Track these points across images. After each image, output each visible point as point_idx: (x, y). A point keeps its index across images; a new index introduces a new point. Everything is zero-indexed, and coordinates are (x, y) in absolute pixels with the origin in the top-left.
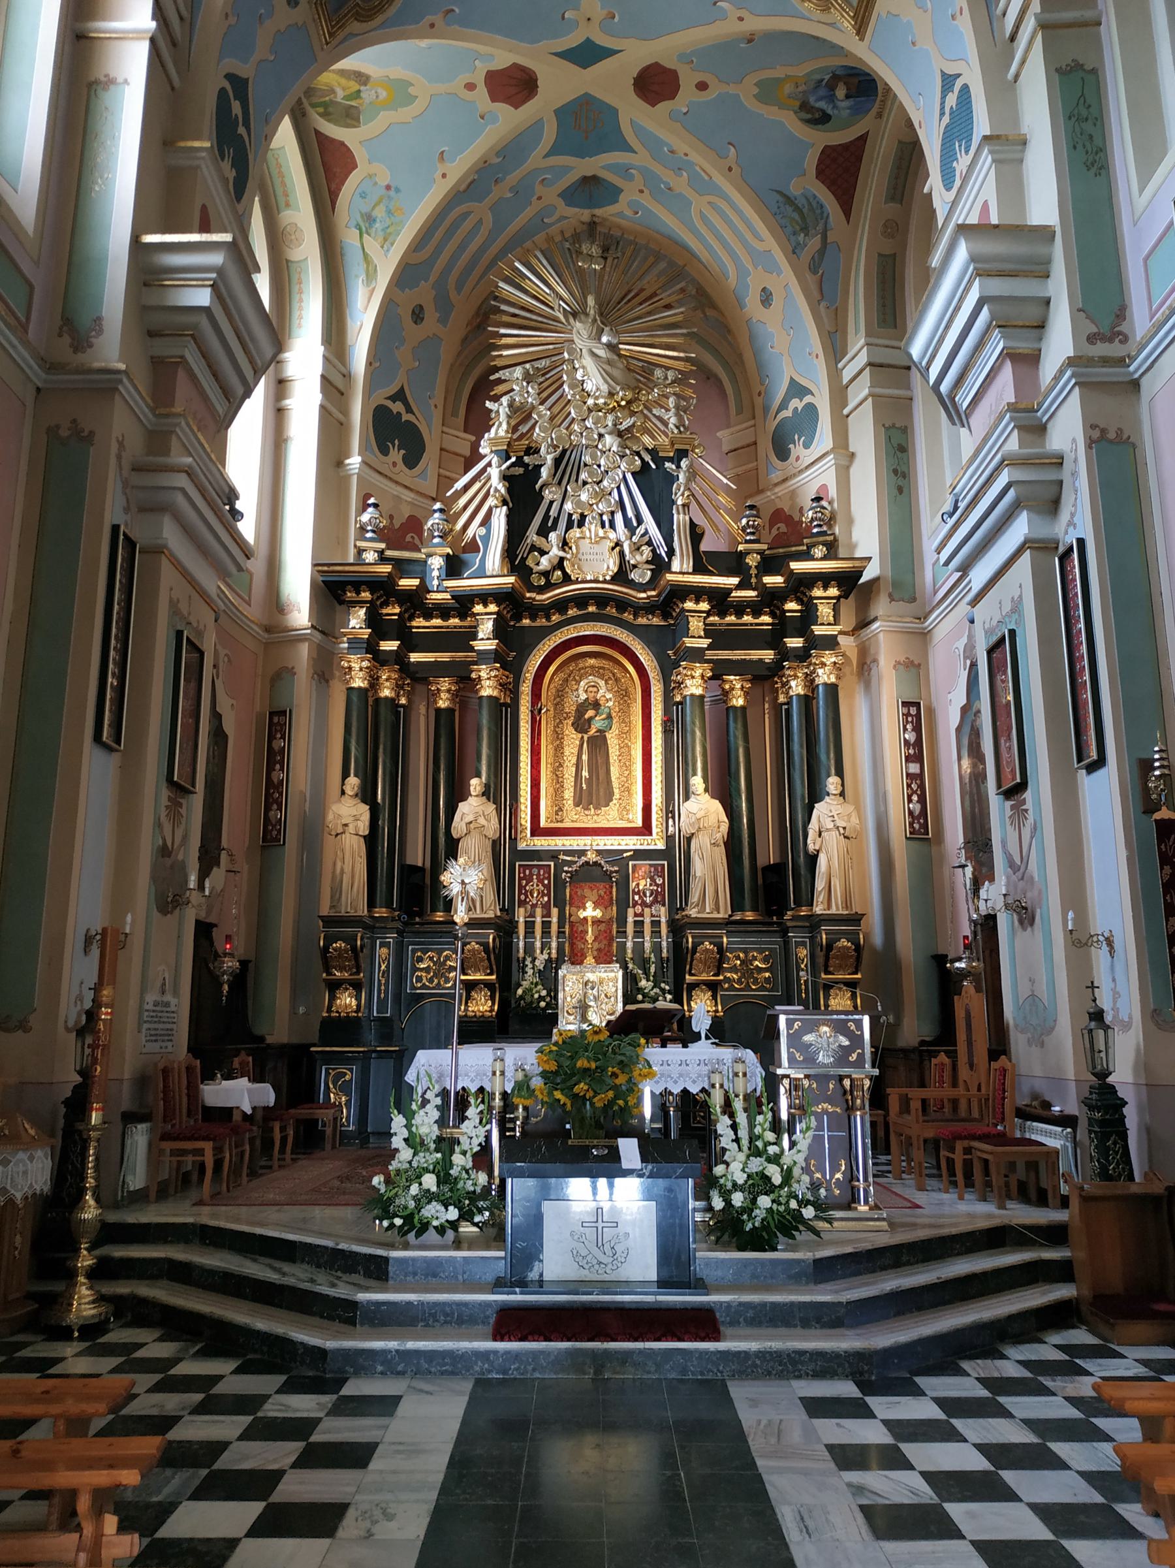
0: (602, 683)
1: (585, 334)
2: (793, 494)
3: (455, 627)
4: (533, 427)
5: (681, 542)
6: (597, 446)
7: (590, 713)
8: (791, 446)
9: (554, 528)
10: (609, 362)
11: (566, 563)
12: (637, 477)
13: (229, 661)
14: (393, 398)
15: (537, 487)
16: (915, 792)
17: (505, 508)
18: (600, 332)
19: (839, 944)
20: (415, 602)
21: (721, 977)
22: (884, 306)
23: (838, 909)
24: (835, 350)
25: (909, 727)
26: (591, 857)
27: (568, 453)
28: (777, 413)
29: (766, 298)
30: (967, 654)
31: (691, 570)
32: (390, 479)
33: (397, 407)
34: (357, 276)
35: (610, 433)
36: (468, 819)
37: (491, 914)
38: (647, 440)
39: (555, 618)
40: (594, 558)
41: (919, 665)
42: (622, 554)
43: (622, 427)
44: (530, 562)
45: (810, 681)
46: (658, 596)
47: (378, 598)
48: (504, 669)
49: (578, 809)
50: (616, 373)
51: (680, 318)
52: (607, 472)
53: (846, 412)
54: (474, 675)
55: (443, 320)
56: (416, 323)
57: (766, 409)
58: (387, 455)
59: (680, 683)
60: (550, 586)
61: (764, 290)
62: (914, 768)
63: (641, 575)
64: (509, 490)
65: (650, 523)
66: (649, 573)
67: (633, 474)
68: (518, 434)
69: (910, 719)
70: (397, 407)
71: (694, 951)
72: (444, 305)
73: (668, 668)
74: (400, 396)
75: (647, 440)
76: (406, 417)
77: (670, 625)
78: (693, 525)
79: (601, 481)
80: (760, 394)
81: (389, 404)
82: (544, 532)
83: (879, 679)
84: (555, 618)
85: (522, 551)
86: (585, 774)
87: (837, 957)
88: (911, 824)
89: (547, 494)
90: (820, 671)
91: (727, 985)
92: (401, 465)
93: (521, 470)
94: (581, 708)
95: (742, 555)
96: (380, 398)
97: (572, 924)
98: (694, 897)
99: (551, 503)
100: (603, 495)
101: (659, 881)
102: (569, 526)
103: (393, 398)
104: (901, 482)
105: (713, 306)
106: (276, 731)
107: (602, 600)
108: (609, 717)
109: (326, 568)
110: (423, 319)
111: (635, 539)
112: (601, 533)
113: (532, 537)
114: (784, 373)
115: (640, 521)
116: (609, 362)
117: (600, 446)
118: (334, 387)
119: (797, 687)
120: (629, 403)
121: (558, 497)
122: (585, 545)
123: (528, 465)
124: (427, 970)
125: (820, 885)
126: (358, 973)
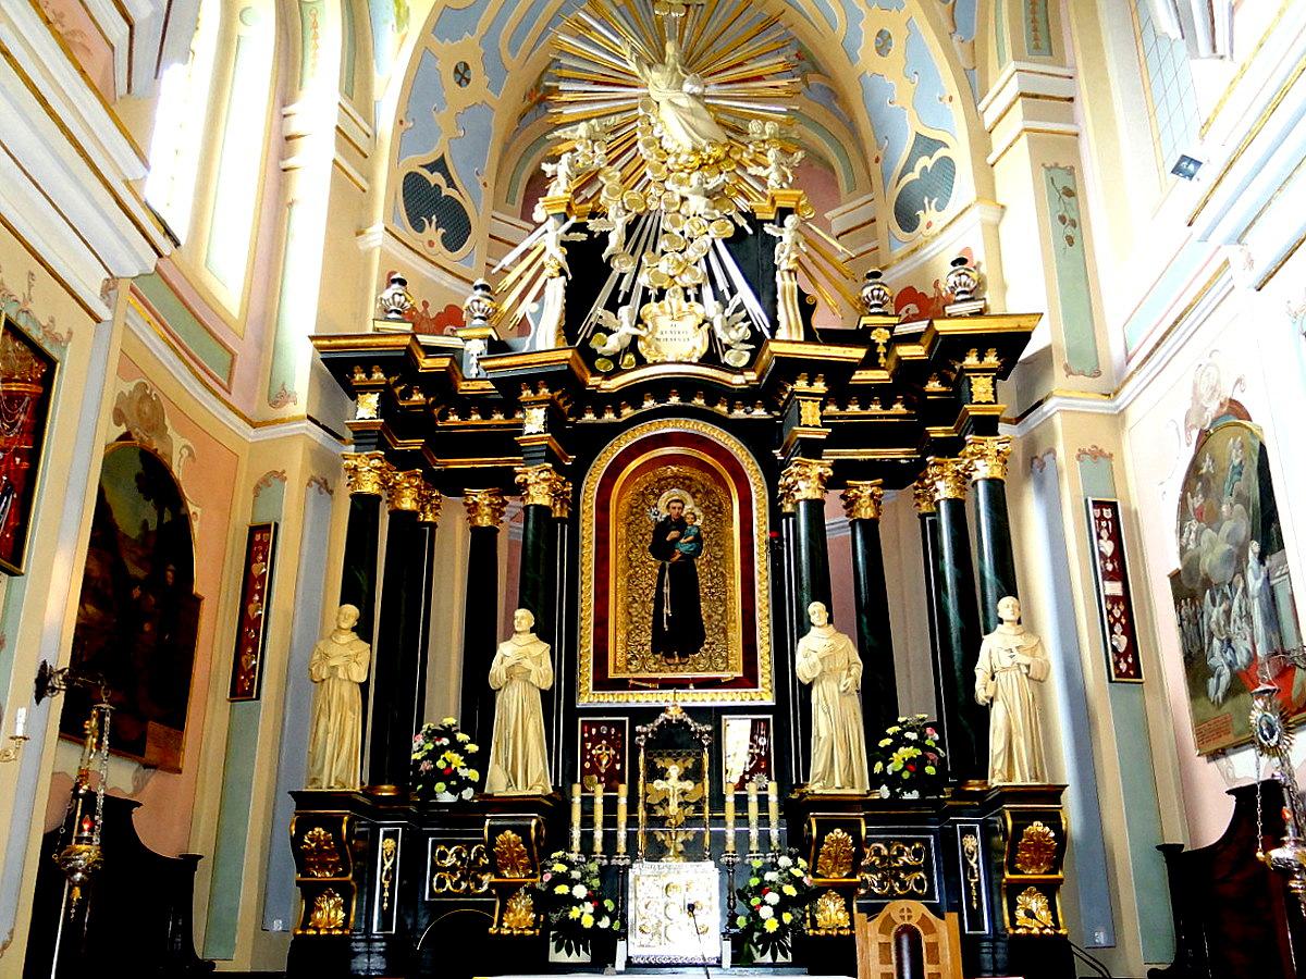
0: (688, 497)
1: (663, 86)
2: (924, 268)
3: (499, 426)
4: (600, 190)
5: (788, 312)
6: (678, 211)
7: (674, 534)
8: (920, 213)
9: (626, 301)
10: (692, 112)
11: (641, 345)
12: (731, 246)
13: (191, 454)
14: (432, 167)
15: (604, 256)
16: (1118, 620)
17: (564, 278)
18: (681, 81)
19: (1030, 829)
20: (443, 385)
21: (858, 879)
22: (1035, 30)
23: (1024, 780)
24: (973, 87)
25: (1104, 534)
26: (674, 714)
27: (643, 220)
28: (900, 179)
29: (883, 42)
30: (1193, 421)
31: (802, 339)
32: (424, 257)
33: (436, 178)
34: (386, 22)
35: (695, 193)
36: (508, 662)
37: (538, 791)
38: (742, 203)
39: (627, 412)
40: (676, 339)
41: (1111, 455)
42: (711, 333)
43: (710, 187)
44: (593, 344)
45: (964, 478)
46: (760, 378)
47: (397, 384)
48: (559, 473)
49: (658, 656)
50: (701, 126)
51: (780, 68)
52: (692, 240)
53: (990, 160)
54: (518, 479)
55: (495, 85)
56: (459, 83)
57: (885, 177)
58: (421, 231)
59: (789, 488)
60: (618, 371)
61: (881, 33)
62: (1114, 588)
63: (738, 357)
64: (568, 258)
65: (745, 294)
66: (748, 354)
67: (726, 241)
68: (581, 198)
69: (1104, 524)
70: (436, 178)
71: (820, 841)
72: (497, 72)
73: (772, 471)
74: (439, 165)
75: (742, 203)
76: (446, 191)
77: (777, 418)
78: (802, 296)
79: (684, 250)
80: (877, 160)
81: (425, 173)
82: (612, 306)
83: (1058, 475)
84: (627, 412)
85: (583, 332)
86: (667, 611)
87: (1027, 848)
88: (1117, 665)
89: (617, 267)
90: (979, 464)
91: (862, 891)
92: (439, 245)
93: (583, 237)
94: (662, 528)
95: (868, 330)
96: (415, 163)
97: (649, 808)
98: (818, 765)
99: (622, 276)
100: (684, 267)
101: (762, 742)
102: (645, 299)
103: (432, 167)
104: (1070, 231)
105: (816, 68)
106: (258, 552)
107: (687, 386)
108: (698, 539)
109: (326, 343)
110: (468, 81)
111: (728, 312)
112: (685, 306)
113: (598, 310)
114: (909, 127)
115: (733, 291)
116: (692, 112)
117: (683, 211)
118: (352, 147)
119: (944, 490)
120: (717, 161)
121: (629, 268)
122: (664, 323)
123: (593, 233)
124: (453, 869)
125: (996, 744)
126: (345, 874)
